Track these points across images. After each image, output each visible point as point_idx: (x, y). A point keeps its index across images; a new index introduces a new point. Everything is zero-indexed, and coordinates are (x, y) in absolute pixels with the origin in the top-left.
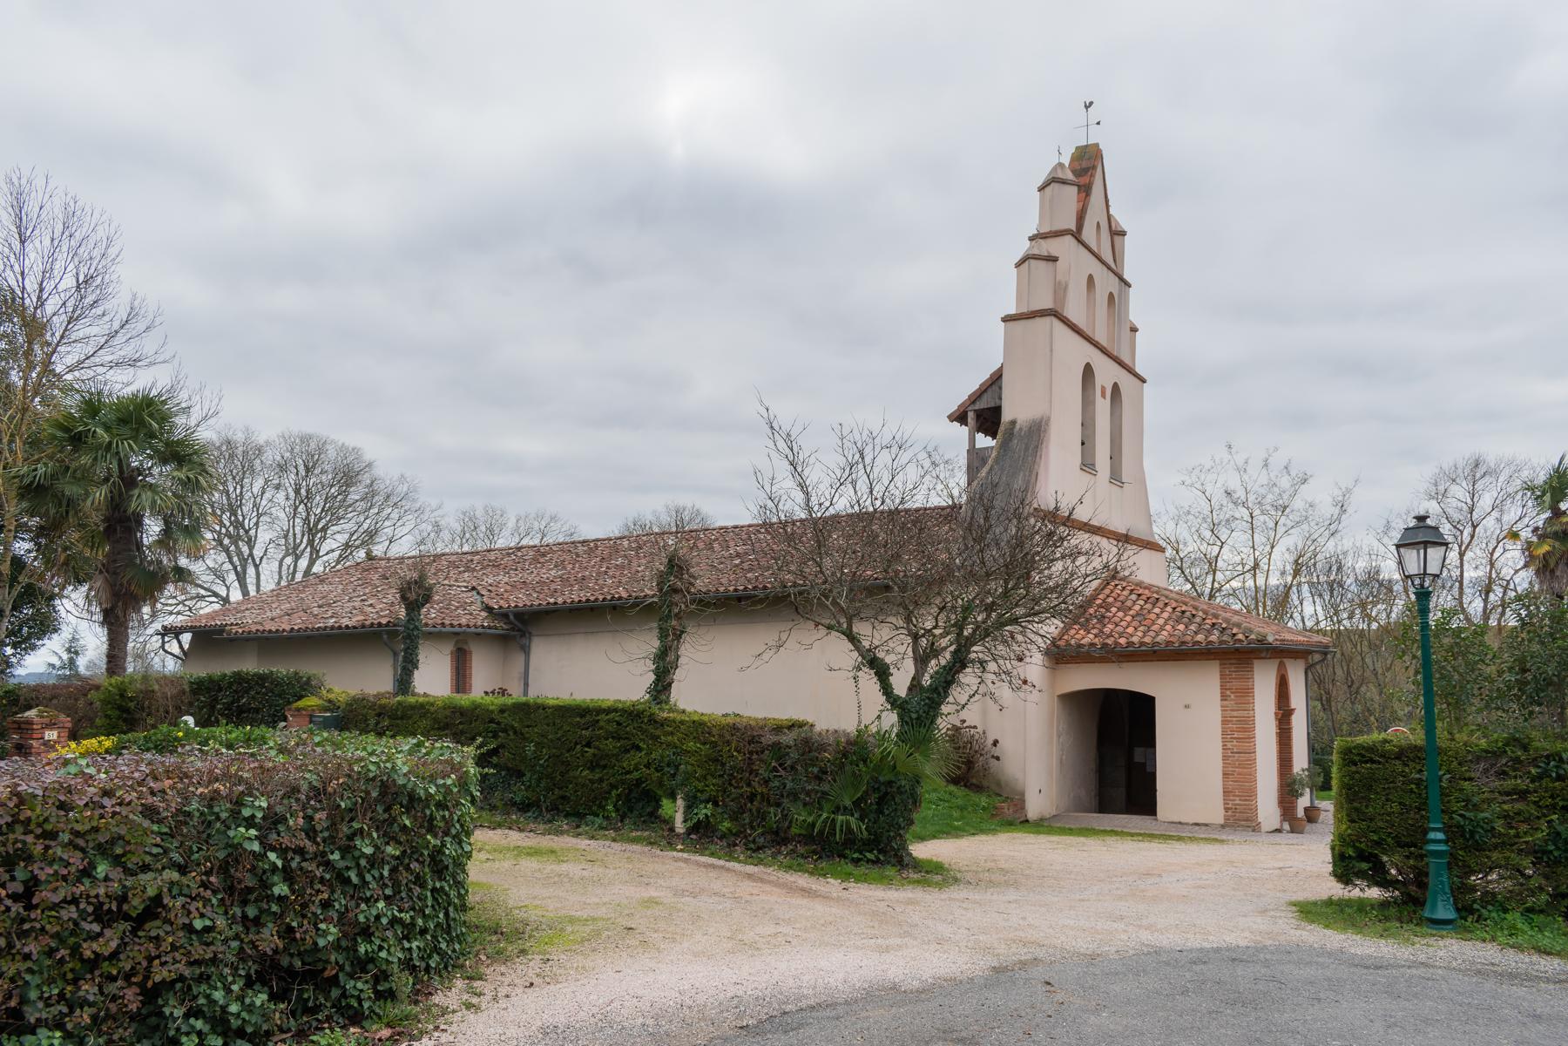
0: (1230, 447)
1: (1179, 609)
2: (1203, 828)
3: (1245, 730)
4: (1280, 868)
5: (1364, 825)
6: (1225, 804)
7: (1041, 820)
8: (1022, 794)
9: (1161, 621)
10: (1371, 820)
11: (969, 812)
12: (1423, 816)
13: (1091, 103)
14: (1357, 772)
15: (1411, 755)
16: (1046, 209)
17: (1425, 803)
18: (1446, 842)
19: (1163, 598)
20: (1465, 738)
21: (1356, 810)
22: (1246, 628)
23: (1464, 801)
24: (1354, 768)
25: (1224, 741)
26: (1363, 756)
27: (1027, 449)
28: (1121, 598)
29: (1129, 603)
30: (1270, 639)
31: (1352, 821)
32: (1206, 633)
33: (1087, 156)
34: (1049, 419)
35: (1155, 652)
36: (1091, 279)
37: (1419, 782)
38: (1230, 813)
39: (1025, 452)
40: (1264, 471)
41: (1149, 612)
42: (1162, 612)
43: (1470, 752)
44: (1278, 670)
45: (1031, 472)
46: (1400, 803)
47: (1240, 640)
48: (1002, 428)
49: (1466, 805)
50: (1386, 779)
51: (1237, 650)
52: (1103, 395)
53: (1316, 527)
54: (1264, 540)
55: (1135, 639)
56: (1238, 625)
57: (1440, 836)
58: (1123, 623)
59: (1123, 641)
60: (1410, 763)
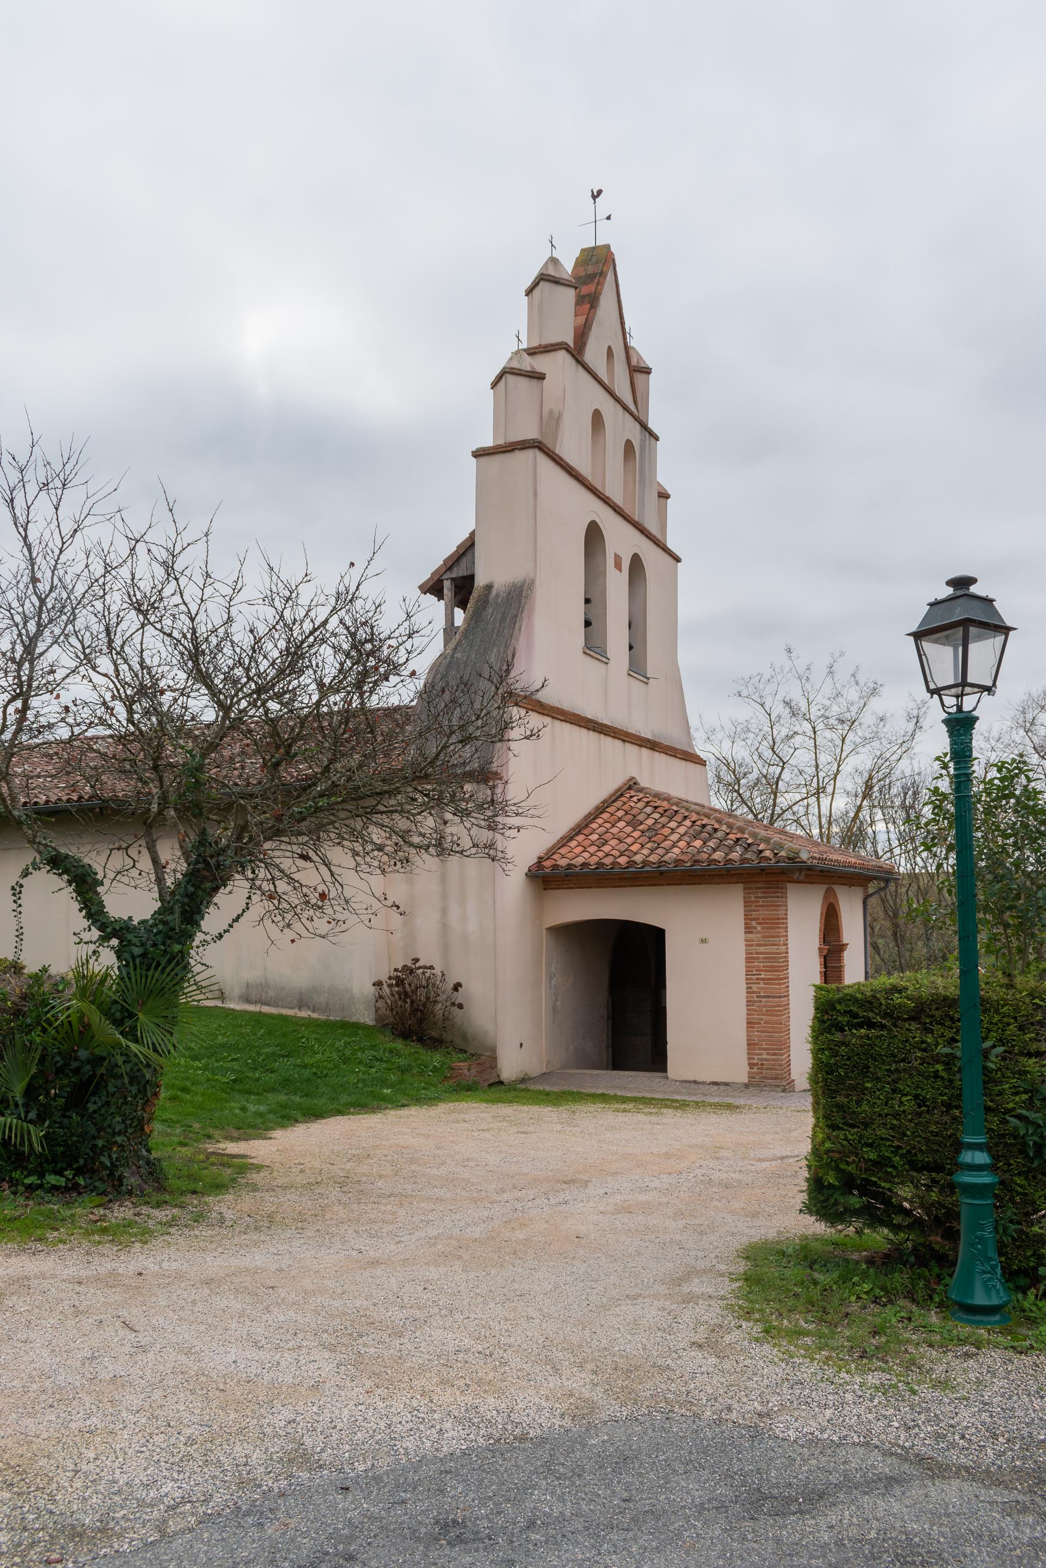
0: (789, 651)
1: (699, 823)
2: (722, 1088)
3: (773, 969)
4: (782, 1158)
5: (852, 1134)
6: (749, 1059)
7: (523, 1080)
8: (494, 1050)
9: (674, 837)
10: (866, 1125)
11: (413, 1075)
12: (954, 1118)
13: (600, 192)
14: (844, 1043)
15: (937, 1014)
16: (537, 317)
17: (959, 1097)
18: (993, 1168)
19: (683, 811)
20: (1033, 983)
21: (840, 1107)
22: (775, 843)
23: (1026, 1092)
24: (838, 1037)
25: (749, 982)
26: (856, 1016)
27: (503, 619)
28: (634, 812)
29: (641, 817)
30: (804, 856)
31: (834, 1127)
32: (727, 850)
33: (594, 260)
34: (533, 582)
35: (662, 873)
36: (597, 416)
37: (949, 1061)
38: (755, 1070)
39: (500, 623)
40: (829, 679)
41: (664, 826)
42: (678, 827)
43: (1039, 1007)
44: (825, 897)
45: (507, 647)
46: (916, 1097)
47: (767, 858)
48: (475, 594)
49: (1031, 1098)
50: (893, 1055)
51: (763, 869)
52: (618, 565)
53: (888, 746)
54: (830, 759)
55: (638, 858)
56: (767, 840)
57: (981, 1158)
58: (629, 840)
59: (623, 860)
60: (936, 1027)
